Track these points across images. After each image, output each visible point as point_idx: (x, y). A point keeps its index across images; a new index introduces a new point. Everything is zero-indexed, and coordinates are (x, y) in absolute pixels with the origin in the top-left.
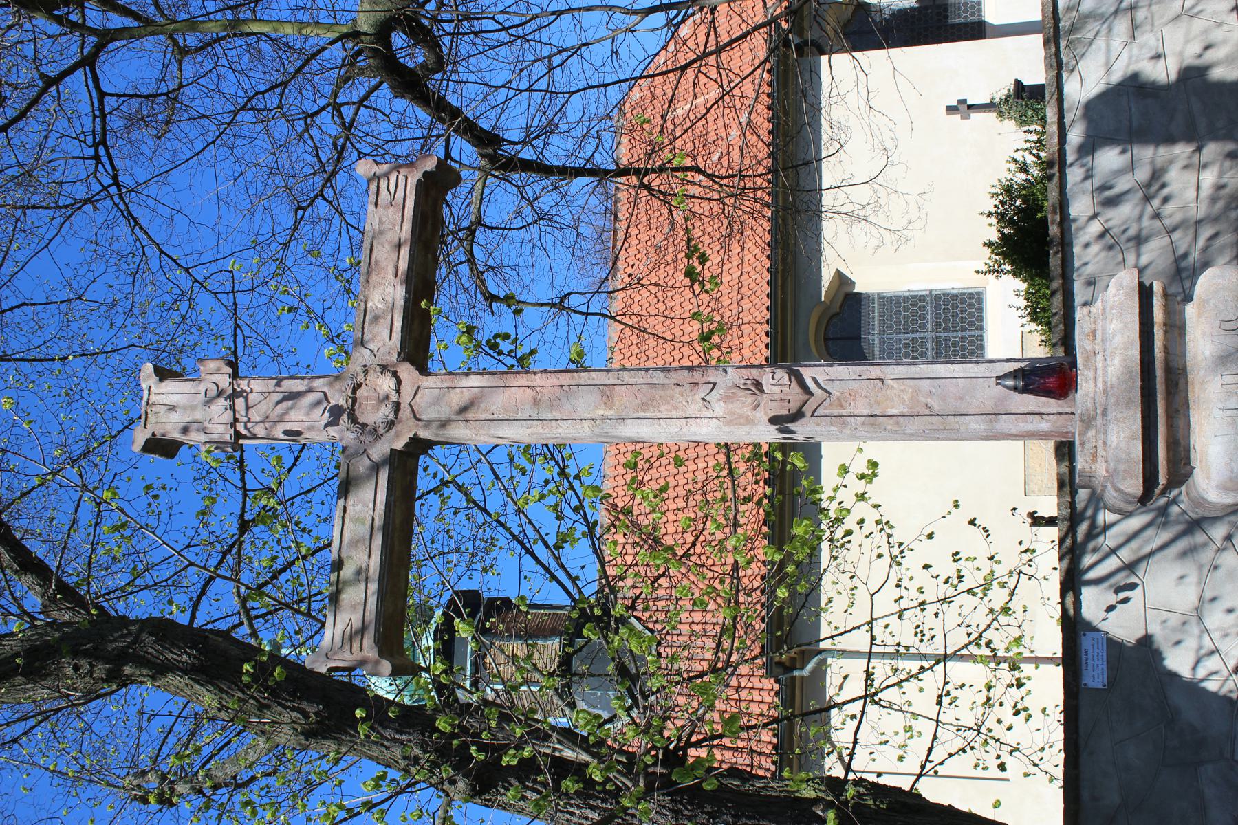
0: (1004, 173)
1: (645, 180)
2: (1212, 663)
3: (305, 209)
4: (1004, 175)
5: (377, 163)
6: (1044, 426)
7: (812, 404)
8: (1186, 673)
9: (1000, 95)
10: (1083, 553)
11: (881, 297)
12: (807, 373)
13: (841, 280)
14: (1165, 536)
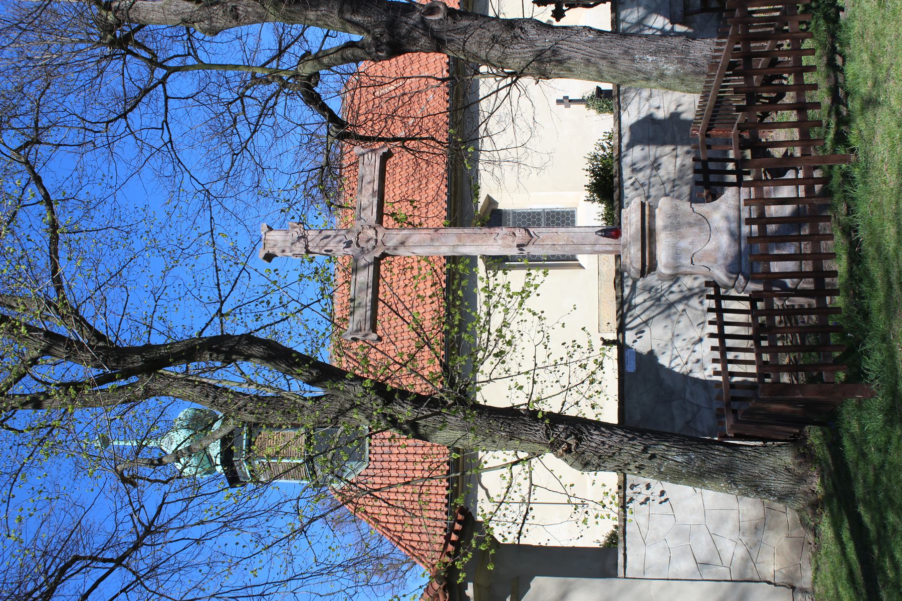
0: (591, 148)
1: (406, 144)
2: (678, 361)
3: (237, 155)
4: (593, 150)
5: (363, 147)
6: (611, 248)
7: (533, 241)
8: (667, 365)
9: (589, 94)
10: (626, 317)
11: (514, 212)
12: (531, 230)
13: (490, 201)
14: (659, 310)
